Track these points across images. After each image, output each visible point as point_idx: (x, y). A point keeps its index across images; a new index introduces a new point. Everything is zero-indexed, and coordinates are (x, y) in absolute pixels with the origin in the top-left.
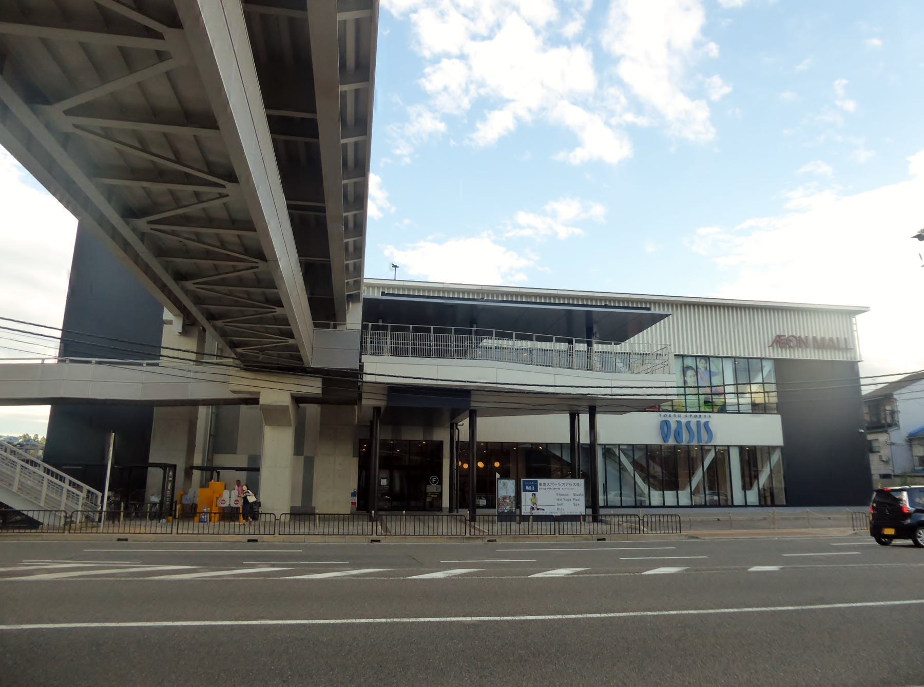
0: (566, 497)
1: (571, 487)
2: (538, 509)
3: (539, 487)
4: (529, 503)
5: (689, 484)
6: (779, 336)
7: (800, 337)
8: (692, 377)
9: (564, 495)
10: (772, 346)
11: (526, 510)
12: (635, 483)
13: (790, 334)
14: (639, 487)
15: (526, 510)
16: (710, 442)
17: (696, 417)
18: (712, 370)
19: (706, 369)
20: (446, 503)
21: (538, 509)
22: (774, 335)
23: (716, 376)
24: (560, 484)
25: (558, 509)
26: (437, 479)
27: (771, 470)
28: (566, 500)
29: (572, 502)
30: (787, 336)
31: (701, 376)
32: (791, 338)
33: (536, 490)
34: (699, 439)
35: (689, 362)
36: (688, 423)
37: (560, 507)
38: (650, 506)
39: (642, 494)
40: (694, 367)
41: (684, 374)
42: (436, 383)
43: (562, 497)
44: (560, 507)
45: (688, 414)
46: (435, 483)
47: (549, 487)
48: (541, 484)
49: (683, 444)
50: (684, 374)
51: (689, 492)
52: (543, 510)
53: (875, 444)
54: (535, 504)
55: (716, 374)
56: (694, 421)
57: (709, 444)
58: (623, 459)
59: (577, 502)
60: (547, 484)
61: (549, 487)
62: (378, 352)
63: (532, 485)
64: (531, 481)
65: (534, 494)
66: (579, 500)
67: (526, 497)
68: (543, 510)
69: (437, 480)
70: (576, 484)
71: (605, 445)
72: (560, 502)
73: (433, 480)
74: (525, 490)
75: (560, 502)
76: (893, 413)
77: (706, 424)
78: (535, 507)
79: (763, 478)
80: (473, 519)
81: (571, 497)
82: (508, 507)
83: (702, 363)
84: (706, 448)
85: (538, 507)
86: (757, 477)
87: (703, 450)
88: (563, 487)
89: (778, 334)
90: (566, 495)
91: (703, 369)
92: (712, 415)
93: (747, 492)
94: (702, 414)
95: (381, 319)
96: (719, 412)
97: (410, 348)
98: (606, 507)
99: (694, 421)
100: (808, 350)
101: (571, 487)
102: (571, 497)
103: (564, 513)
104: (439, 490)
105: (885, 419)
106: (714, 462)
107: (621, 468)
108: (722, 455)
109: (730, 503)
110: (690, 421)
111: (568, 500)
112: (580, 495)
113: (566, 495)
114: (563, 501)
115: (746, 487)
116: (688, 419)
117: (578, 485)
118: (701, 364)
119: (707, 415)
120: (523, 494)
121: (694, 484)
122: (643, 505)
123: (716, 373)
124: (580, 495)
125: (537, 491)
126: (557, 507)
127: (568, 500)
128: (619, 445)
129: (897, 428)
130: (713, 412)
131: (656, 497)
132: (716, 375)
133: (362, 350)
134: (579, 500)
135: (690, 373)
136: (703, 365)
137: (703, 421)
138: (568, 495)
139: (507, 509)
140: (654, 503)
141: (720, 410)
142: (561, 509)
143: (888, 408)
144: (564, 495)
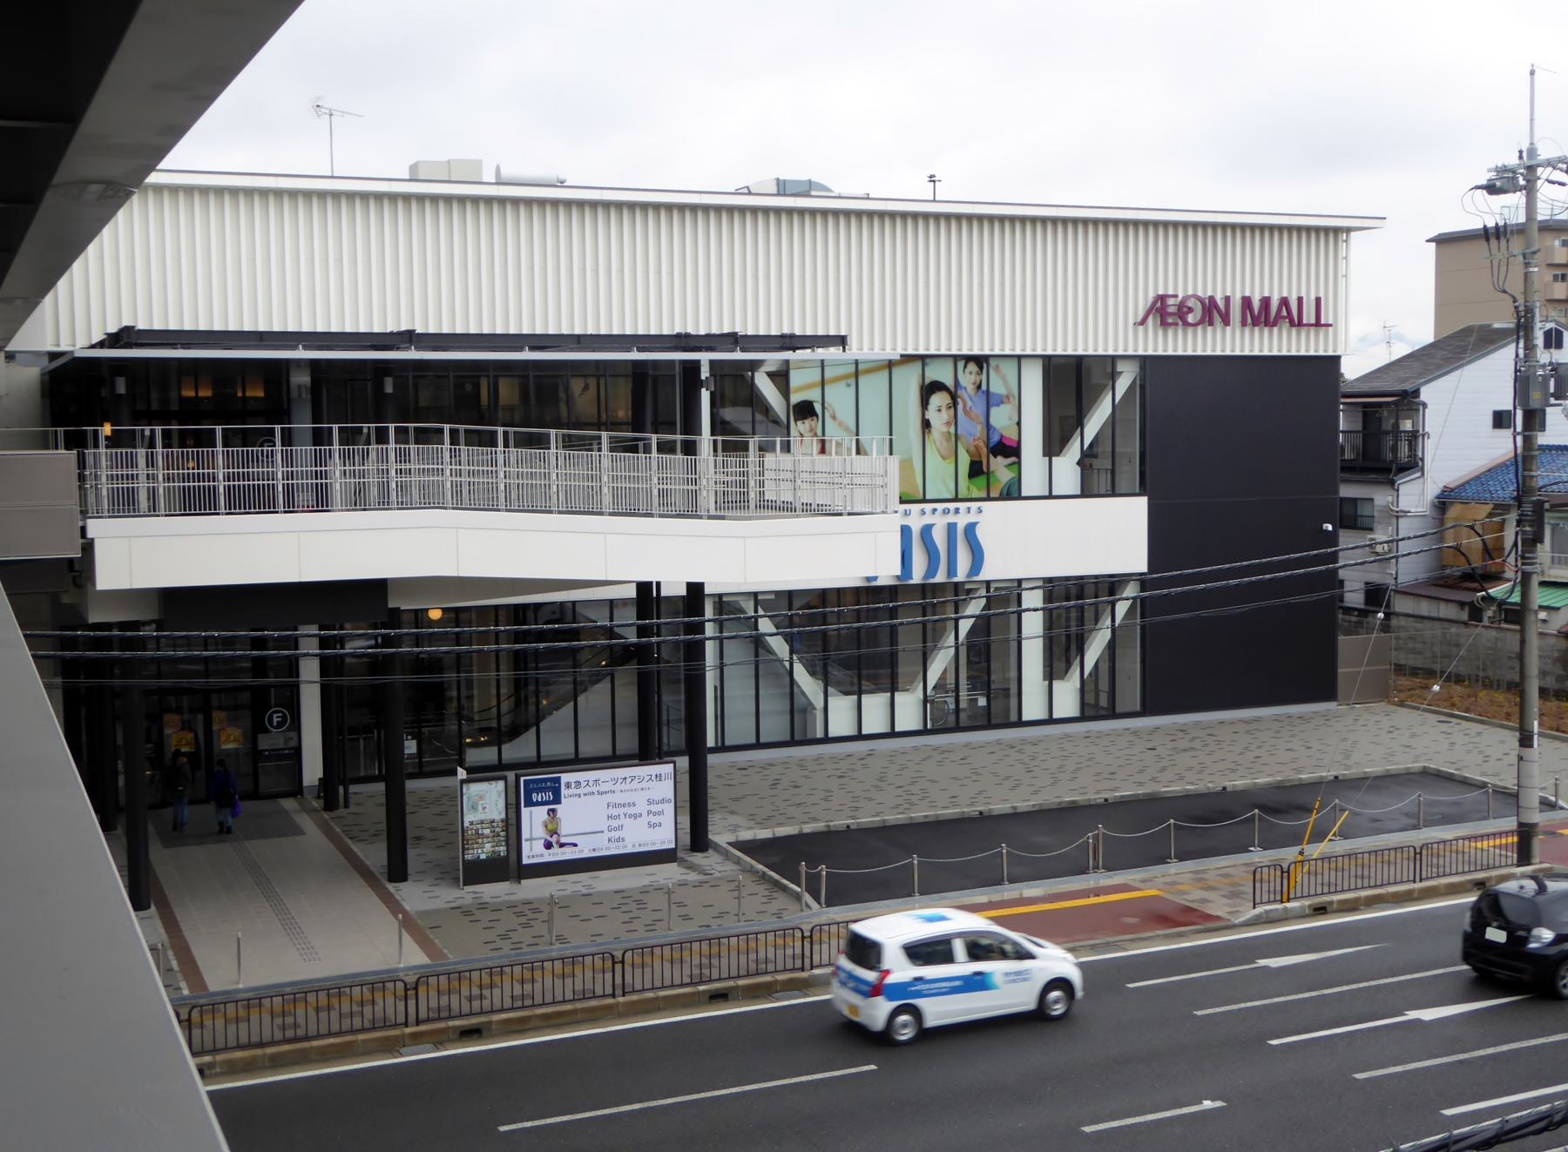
0: (632, 811)
1: (641, 785)
2: (562, 845)
3: (564, 791)
4: (540, 832)
5: (921, 676)
6: (1162, 298)
7: (1212, 299)
8: (944, 409)
9: (624, 805)
10: (1143, 322)
11: (533, 852)
12: (792, 681)
13: (1190, 292)
14: (803, 693)
15: (533, 852)
16: (977, 574)
17: (946, 512)
18: (992, 389)
19: (979, 387)
20: (312, 769)
21: (562, 845)
22: (1151, 296)
23: (1002, 406)
24: (615, 781)
25: (610, 840)
26: (284, 714)
27: (1114, 630)
28: (630, 817)
29: (645, 820)
30: (1181, 296)
31: (965, 406)
32: (1190, 304)
33: (557, 800)
34: (952, 570)
35: (943, 374)
36: (927, 530)
37: (616, 834)
38: (827, 740)
39: (808, 707)
40: (949, 382)
41: (925, 403)
42: (316, 689)
43: (621, 811)
44: (616, 834)
45: (928, 507)
46: (280, 725)
47: (588, 790)
48: (568, 786)
49: (911, 582)
50: (925, 403)
51: (922, 697)
52: (575, 845)
53: (1363, 510)
54: (554, 832)
55: (1001, 401)
56: (940, 524)
57: (975, 579)
58: (766, 626)
59: (655, 819)
60: (583, 784)
61: (588, 790)
62: (125, 504)
63: (548, 789)
64: (546, 780)
65: (553, 811)
66: (661, 813)
67: (533, 819)
68: (575, 845)
69: (284, 717)
70: (653, 777)
71: (720, 596)
72: (615, 823)
73: (275, 720)
74: (529, 803)
75: (615, 823)
76: (1414, 437)
77: (971, 529)
78: (553, 840)
79: (1094, 650)
80: (398, 871)
81: (642, 807)
82: (488, 847)
83: (971, 373)
84: (967, 586)
85: (563, 840)
86: (1081, 652)
87: (959, 592)
88: (624, 787)
89: (1161, 292)
90: (629, 805)
91: (971, 388)
92: (985, 505)
93: (1056, 684)
94: (962, 506)
95: (120, 375)
96: (1001, 498)
97: (221, 490)
98: (722, 748)
99: (940, 524)
100: (1228, 329)
101: (641, 785)
102: (642, 807)
103: (625, 847)
104: (293, 743)
105: (1395, 449)
106: (983, 625)
107: (758, 642)
108: (1006, 597)
109: (1014, 718)
110: (932, 525)
111: (635, 816)
112: (663, 801)
113: (629, 805)
114: (622, 821)
115: (1052, 672)
116: (927, 520)
117: (659, 777)
118: (968, 378)
119: (974, 505)
120: (525, 811)
121: (933, 676)
122: (809, 736)
123: (1001, 396)
124: (663, 801)
125: (560, 803)
126: (607, 835)
127: (635, 816)
128: (755, 594)
129: (1418, 474)
130: (988, 499)
131: (840, 714)
132: (1002, 403)
133: (84, 514)
134: (661, 813)
135: (938, 400)
136: (973, 378)
137: (962, 521)
138: (634, 805)
139: (484, 851)
140: (834, 731)
141: (1005, 492)
142: (618, 840)
143: (1407, 425)
144: (624, 805)
